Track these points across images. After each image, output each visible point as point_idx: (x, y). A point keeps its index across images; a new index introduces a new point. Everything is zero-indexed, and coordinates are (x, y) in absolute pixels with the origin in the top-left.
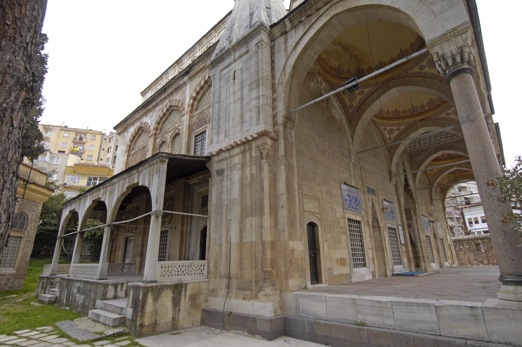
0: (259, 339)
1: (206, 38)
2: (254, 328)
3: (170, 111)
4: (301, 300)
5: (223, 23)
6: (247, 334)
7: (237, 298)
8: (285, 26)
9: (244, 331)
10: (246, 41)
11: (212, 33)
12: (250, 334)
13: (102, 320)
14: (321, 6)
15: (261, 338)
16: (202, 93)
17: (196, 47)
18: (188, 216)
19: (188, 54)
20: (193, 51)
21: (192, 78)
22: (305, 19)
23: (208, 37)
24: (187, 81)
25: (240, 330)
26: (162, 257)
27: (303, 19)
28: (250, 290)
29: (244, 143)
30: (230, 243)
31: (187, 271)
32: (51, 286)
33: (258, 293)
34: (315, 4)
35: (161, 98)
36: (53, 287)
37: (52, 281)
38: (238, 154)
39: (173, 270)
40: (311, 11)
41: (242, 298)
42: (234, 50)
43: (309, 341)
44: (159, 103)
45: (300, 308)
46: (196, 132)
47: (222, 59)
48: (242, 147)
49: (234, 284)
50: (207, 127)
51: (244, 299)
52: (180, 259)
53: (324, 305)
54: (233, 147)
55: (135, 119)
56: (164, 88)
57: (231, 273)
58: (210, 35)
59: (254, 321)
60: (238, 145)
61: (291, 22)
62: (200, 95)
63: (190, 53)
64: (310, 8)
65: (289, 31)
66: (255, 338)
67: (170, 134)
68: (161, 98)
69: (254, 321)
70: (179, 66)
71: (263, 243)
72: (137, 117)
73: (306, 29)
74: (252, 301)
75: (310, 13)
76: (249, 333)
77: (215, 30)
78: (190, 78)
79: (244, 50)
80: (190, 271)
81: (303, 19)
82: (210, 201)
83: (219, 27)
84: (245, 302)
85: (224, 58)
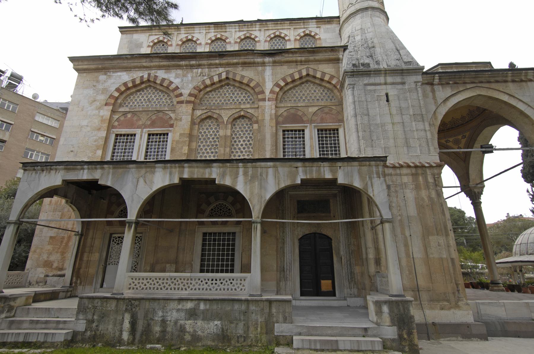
0: (477, 341)
1: (274, 24)
2: (469, 333)
3: (223, 83)
4: (482, 307)
5: (304, 22)
6: (461, 339)
7: (432, 308)
8: (434, 79)
9: (457, 337)
10: (402, 73)
11: (284, 23)
12: (465, 338)
13: (341, 346)
14: (468, 82)
15: (479, 340)
16: (291, 85)
17: (255, 25)
18: (341, 222)
19: (239, 26)
20: (248, 25)
21: (277, 63)
22: (452, 84)
23: (277, 24)
24: (269, 62)
25: (453, 337)
26: (134, 269)
27: (451, 82)
28: (448, 301)
29: (416, 167)
30: (413, 258)
31: (239, 285)
32: (8, 314)
33: (458, 303)
34: (464, 78)
35: (213, 62)
36: (12, 314)
37: (12, 303)
38: (407, 175)
39: (194, 286)
40: (460, 81)
41: (439, 308)
42: (386, 74)
43: (502, 337)
44: (204, 65)
45: (482, 313)
46: (286, 127)
47: (367, 74)
48: (414, 170)
49: (424, 296)
50: (307, 126)
51: (442, 309)
52: (202, 271)
53: (503, 309)
54: (401, 166)
55: (139, 64)
56: (221, 53)
57: (419, 286)
58: (281, 24)
59: (468, 327)
60: (409, 166)
61: (440, 79)
62: (288, 87)
63: (242, 26)
64: (459, 78)
65: (436, 85)
66: (472, 341)
67: (230, 113)
68: (213, 62)
69: (468, 327)
70: (216, 31)
71: (452, 260)
72: (145, 64)
73: (455, 92)
74: (452, 310)
75: (458, 82)
76: (463, 338)
77: (290, 23)
78: (274, 62)
79: (398, 79)
80: (194, 286)
81: (451, 82)
82: (49, 189)
83: (297, 23)
84: (443, 312)
85: (370, 74)
